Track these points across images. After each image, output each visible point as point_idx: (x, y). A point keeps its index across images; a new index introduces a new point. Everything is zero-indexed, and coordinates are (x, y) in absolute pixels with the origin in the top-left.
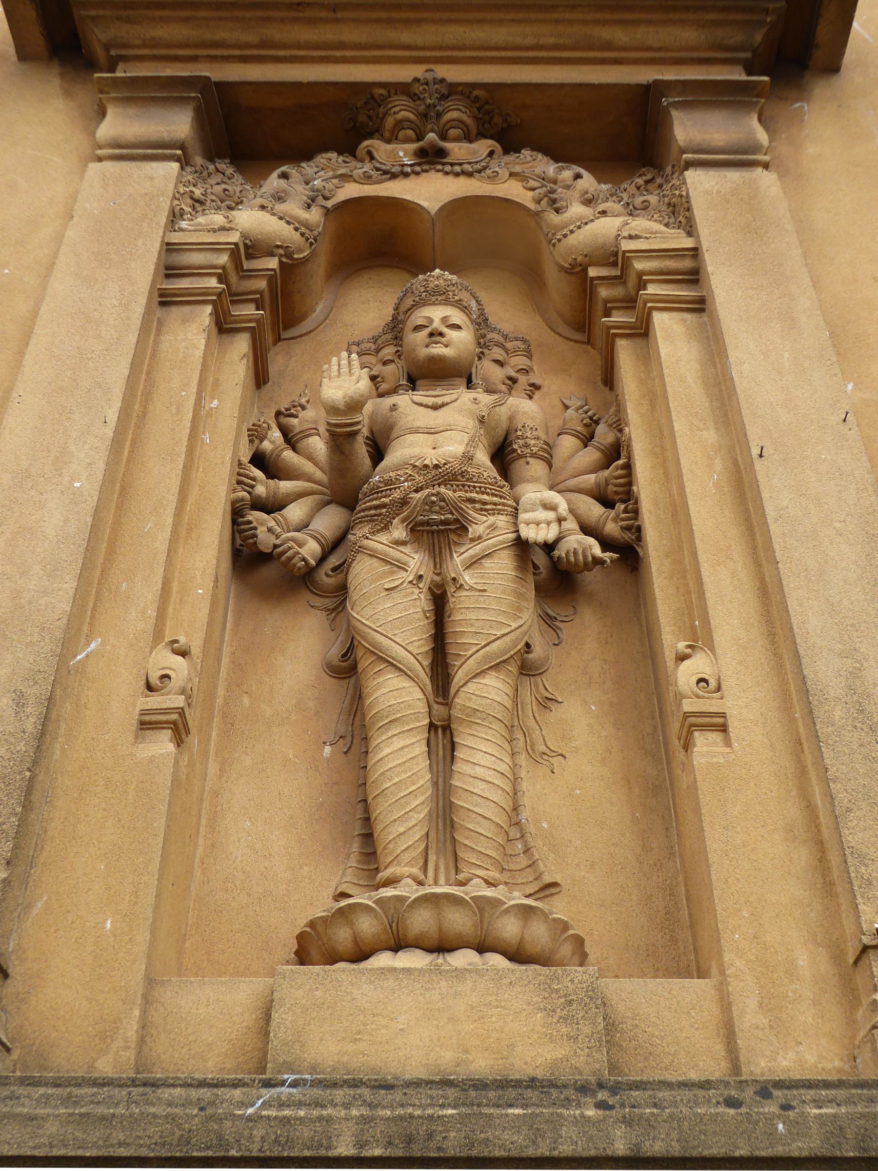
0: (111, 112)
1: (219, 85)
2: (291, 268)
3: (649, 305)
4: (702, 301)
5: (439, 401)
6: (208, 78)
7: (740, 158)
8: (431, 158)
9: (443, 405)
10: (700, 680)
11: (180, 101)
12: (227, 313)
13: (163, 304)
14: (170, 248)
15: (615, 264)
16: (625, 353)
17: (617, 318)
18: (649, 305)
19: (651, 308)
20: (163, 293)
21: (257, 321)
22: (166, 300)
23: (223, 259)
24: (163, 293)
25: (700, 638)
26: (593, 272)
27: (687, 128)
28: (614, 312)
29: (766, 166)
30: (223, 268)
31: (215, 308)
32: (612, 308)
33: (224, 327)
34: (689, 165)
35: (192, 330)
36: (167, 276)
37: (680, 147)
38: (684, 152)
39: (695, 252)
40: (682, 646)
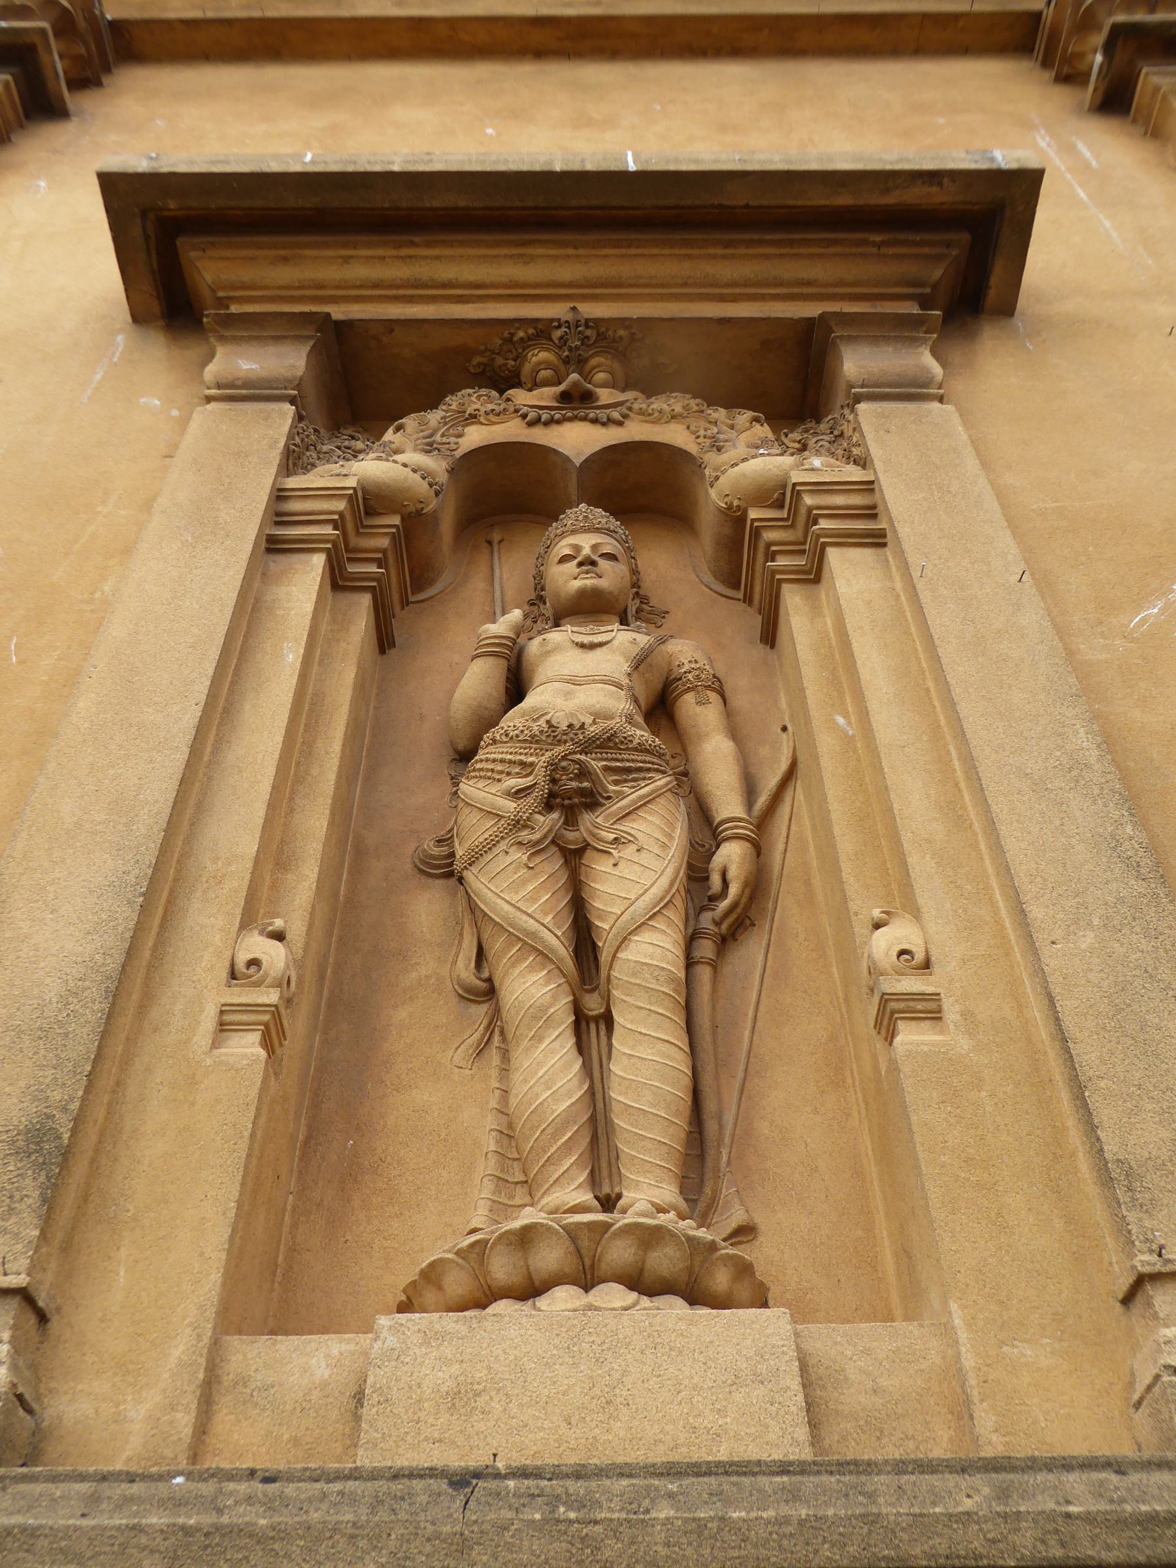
0: (220, 351)
1: (338, 324)
2: (415, 524)
3: (822, 540)
4: (882, 534)
5: (597, 639)
6: (328, 315)
7: (911, 391)
8: (577, 402)
9: (601, 645)
10: (902, 952)
11: (298, 338)
12: (342, 568)
13: (269, 551)
14: (280, 495)
15: (780, 504)
16: (793, 599)
17: (782, 561)
18: (822, 540)
19: (824, 545)
20: (271, 539)
21: (378, 580)
22: (273, 546)
23: (341, 505)
24: (271, 539)
25: (903, 900)
26: (753, 514)
27: (855, 363)
28: (778, 557)
29: (941, 399)
30: (341, 514)
31: (329, 560)
32: (775, 553)
33: (338, 581)
34: (858, 399)
35: (303, 582)
36: (277, 523)
37: (849, 381)
38: (853, 387)
39: (868, 487)
40: (876, 913)
